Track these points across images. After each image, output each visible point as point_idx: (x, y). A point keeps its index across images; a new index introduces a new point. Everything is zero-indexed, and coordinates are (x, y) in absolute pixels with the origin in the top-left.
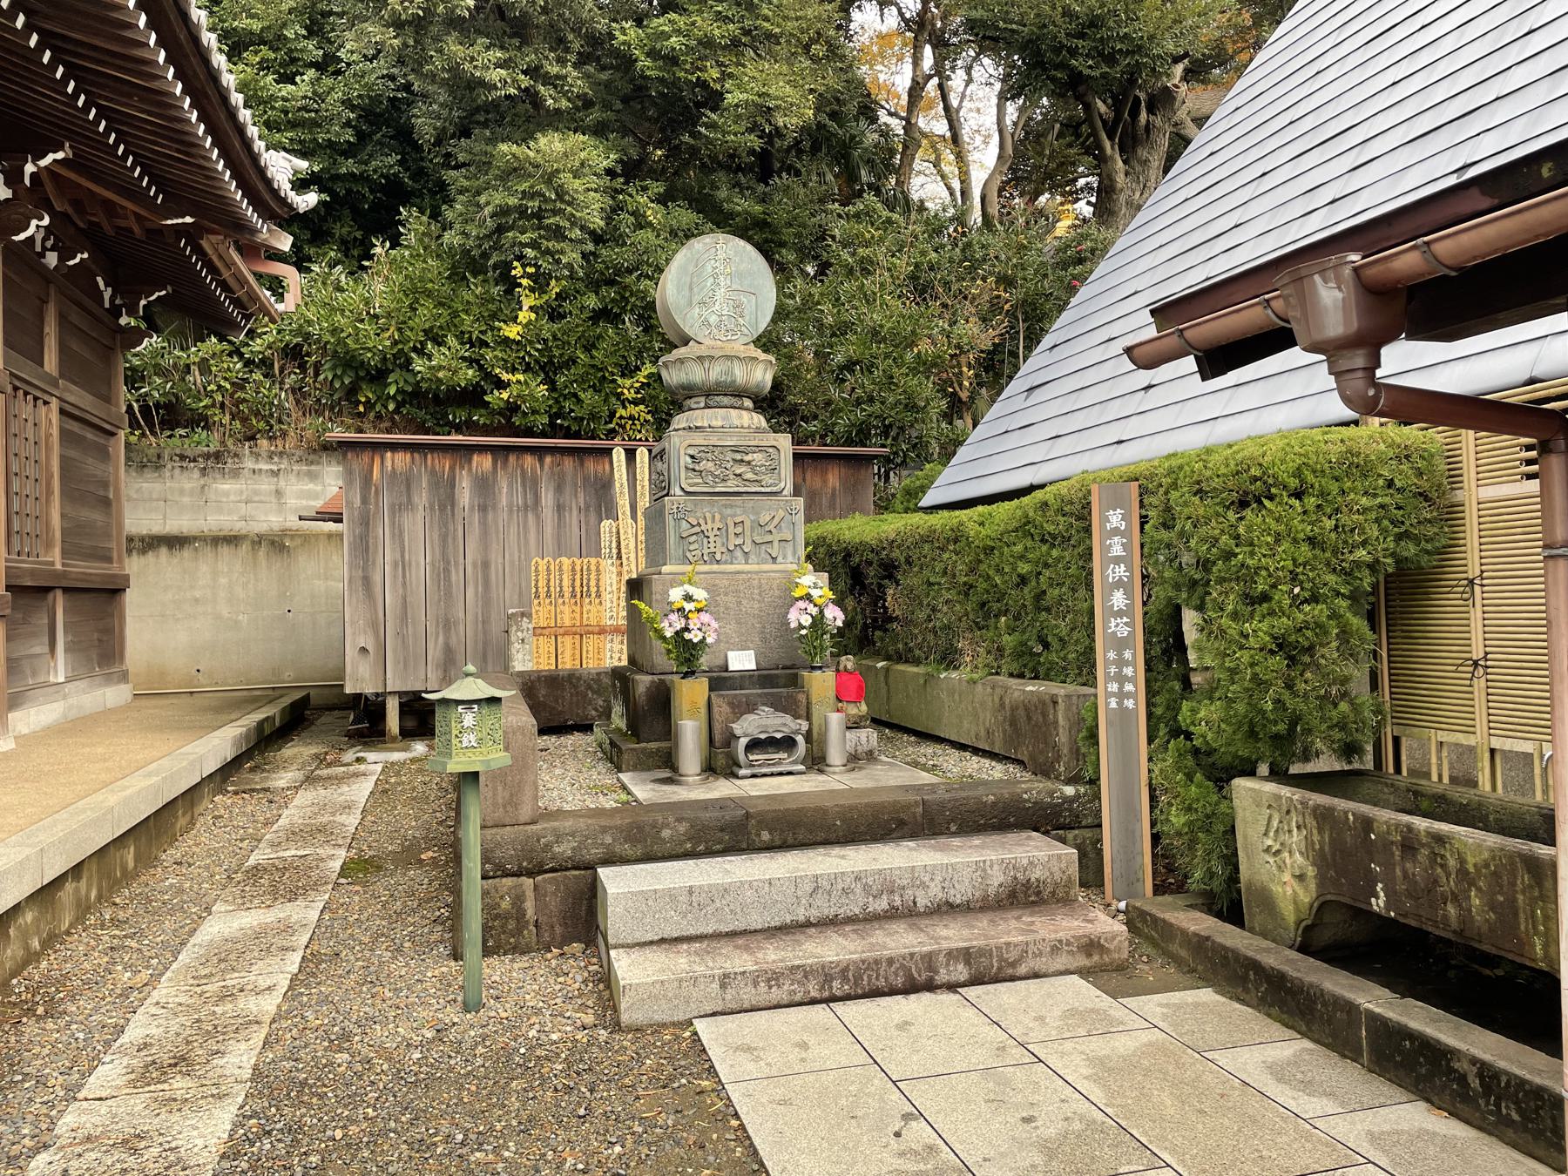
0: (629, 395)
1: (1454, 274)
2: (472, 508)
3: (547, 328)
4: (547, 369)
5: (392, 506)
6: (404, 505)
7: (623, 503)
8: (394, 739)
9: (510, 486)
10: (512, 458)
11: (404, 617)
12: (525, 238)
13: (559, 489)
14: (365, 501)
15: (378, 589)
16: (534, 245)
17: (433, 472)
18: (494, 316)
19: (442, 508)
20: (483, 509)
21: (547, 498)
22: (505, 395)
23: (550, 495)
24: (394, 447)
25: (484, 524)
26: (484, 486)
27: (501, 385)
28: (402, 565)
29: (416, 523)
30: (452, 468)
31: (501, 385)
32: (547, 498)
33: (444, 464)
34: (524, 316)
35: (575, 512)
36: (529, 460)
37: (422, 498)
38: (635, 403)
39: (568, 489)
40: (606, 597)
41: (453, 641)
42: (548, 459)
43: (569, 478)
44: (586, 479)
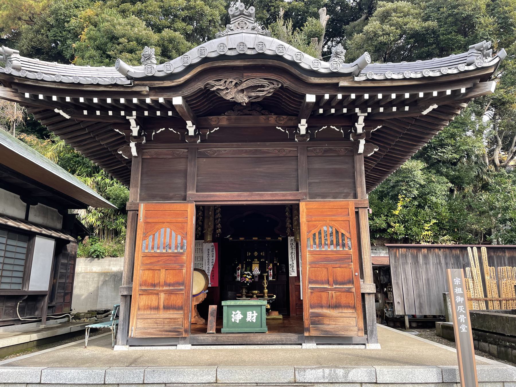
0: (426, 228)
1: (470, 47)
2: (423, 264)
3: (405, 211)
4: (404, 222)
5: (402, 263)
6: (405, 263)
7: (472, 262)
8: (408, 329)
9: (432, 257)
10: (432, 250)
11: (408, 294)
12: (403, 188)
13: (446, 258)
14: (395, 262)
15: (401, 286)
16: (406, 190)
17: (412, 254)
18: (390, 208)
19: (415, 264)
20: (426, 264)
21: (421, 260)
22: (393, 230)
23: (444, 260)
24: (402, 247)
25: (426, 268)
26: (425, 257)
27: (392, 227)
28: (406, 279)
29: (409, 268)
30: (417, 253)
31: (392, 227)
32: (443, 261)
33: (415, 251)
34: (400, 208)
35: (451, 265)
36: (437, 250)
37: (410, 260)
38: (428, 230)
39: (448, 258)
40: (471, 290)
41: (421, 301)
42: (442, 250)
43: (448, 255)
44: (453, 255)
